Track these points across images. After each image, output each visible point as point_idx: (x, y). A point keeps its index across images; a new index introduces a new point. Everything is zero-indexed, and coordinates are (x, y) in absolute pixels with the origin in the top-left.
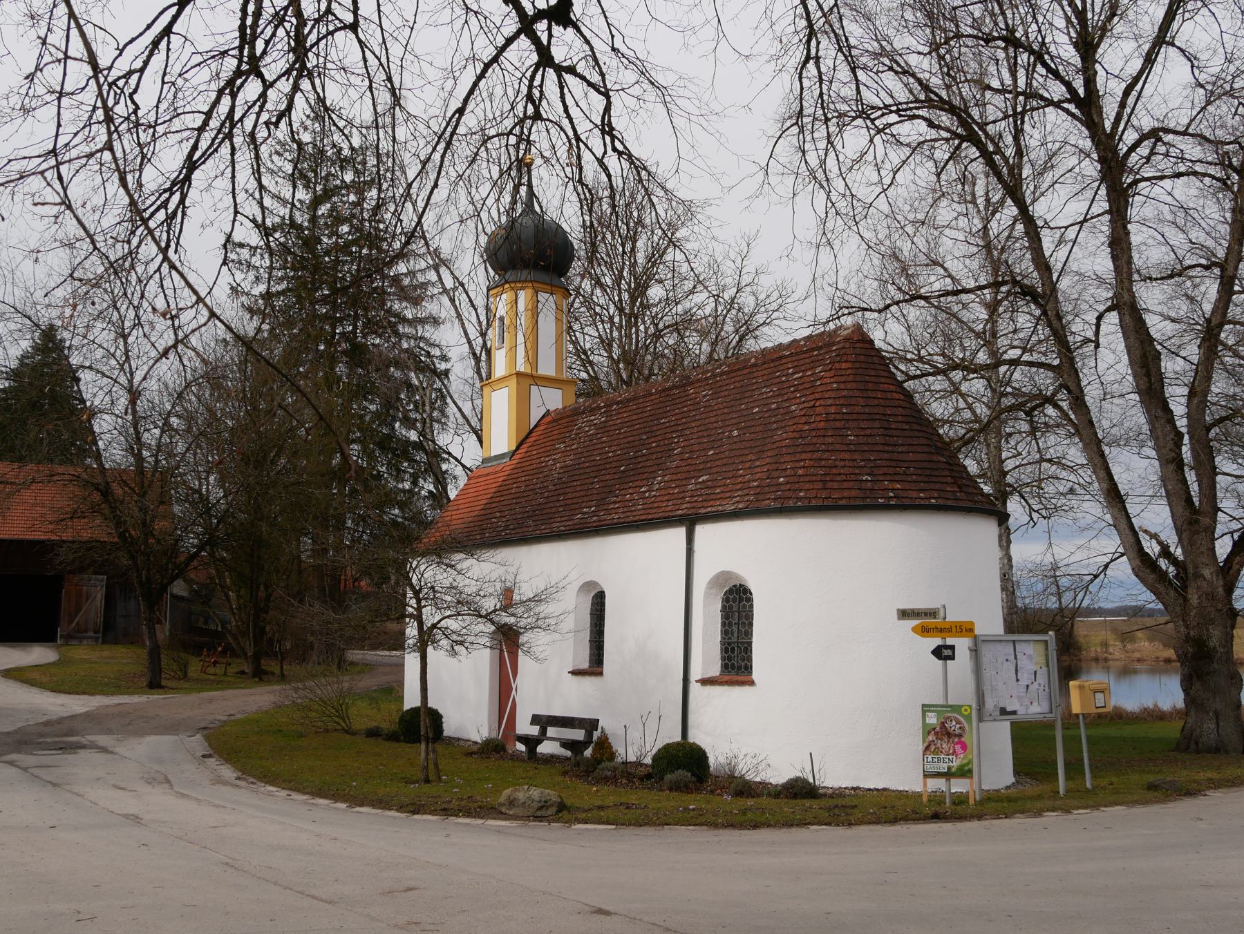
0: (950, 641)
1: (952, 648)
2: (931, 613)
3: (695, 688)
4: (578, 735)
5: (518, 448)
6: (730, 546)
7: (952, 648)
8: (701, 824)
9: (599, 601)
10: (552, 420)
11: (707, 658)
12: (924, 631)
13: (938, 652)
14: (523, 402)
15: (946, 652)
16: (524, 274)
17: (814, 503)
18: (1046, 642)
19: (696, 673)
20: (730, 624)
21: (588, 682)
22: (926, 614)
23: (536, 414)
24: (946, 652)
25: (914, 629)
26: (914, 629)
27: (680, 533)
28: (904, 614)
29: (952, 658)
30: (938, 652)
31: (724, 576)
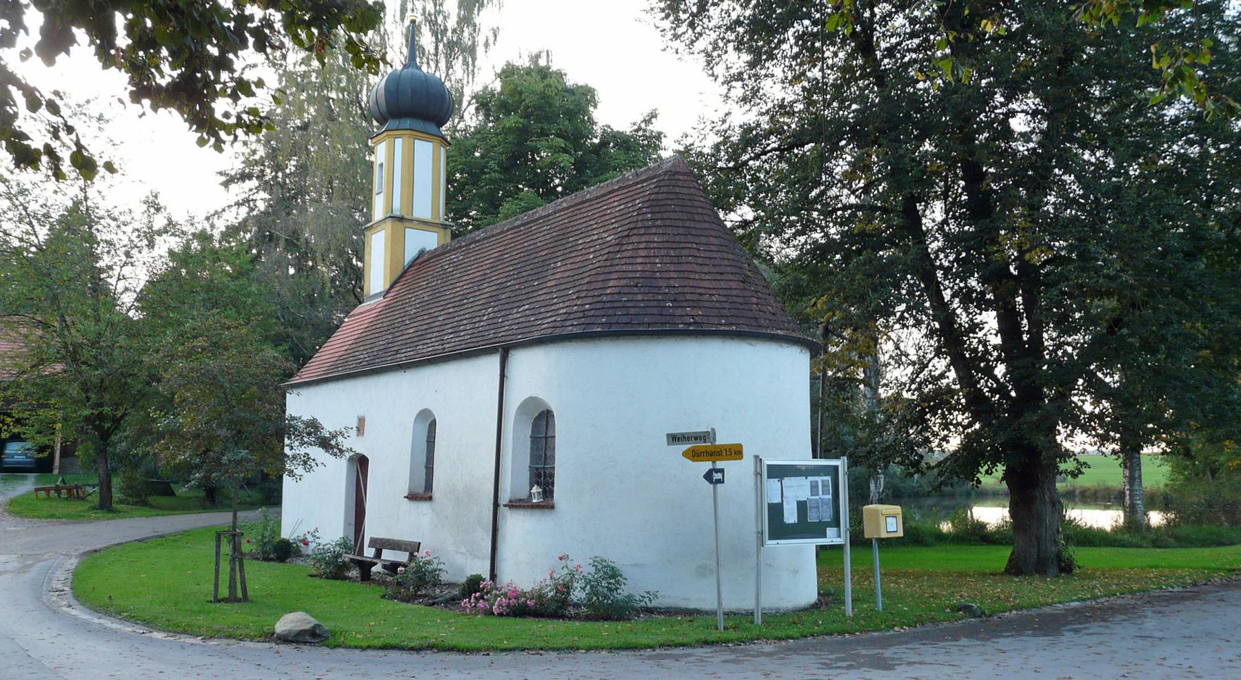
0: (720, 465)
1: (722, 471)
2: (697, 437)
3: (503, 511)
4: (402, 557)
5: (392, 287)
6: (537, 372)
7: (722, 471)
8: (670, 612)
9: (433, 424)
10: (424, 260)
11: (516, 481)
12: (694, 455)
13: (708, 476)
14: (396, 244)
15: (717, 476)
16: (407, 123)
17: (614, 328)
18: (836, 468)
19: (505, 498)
20: (538, 449)
21: (424, 506)
22: (696, 439)
23: (410, 254)
24: (717, 476)
25: (685, 454)
26: (685, 454)
27: (495, 360)
28: (674, 439)
29: (721, 481)
30: (708, 476)
31: (531, 402)
